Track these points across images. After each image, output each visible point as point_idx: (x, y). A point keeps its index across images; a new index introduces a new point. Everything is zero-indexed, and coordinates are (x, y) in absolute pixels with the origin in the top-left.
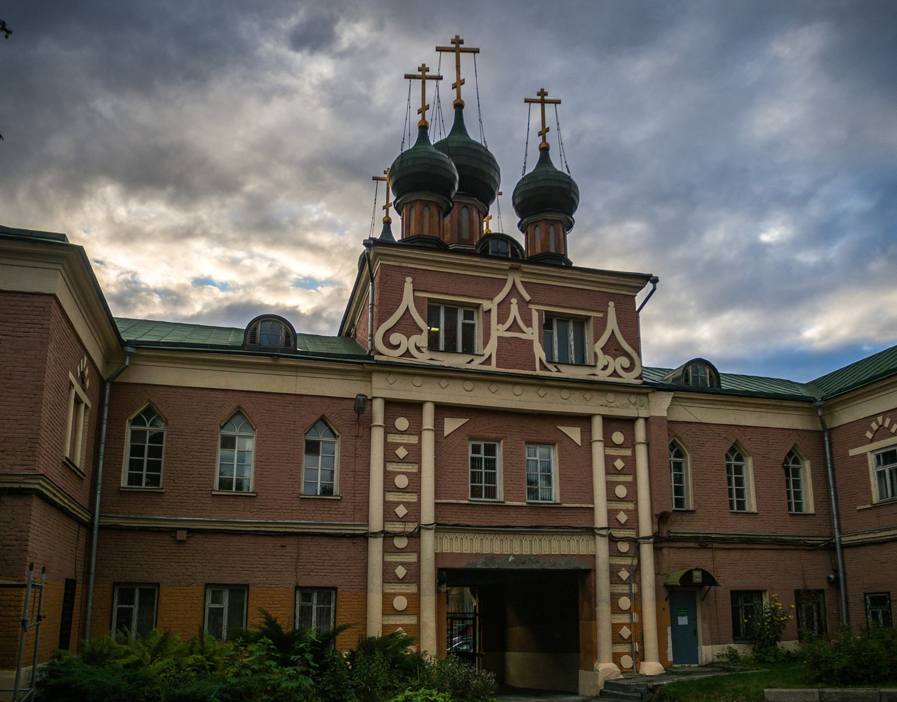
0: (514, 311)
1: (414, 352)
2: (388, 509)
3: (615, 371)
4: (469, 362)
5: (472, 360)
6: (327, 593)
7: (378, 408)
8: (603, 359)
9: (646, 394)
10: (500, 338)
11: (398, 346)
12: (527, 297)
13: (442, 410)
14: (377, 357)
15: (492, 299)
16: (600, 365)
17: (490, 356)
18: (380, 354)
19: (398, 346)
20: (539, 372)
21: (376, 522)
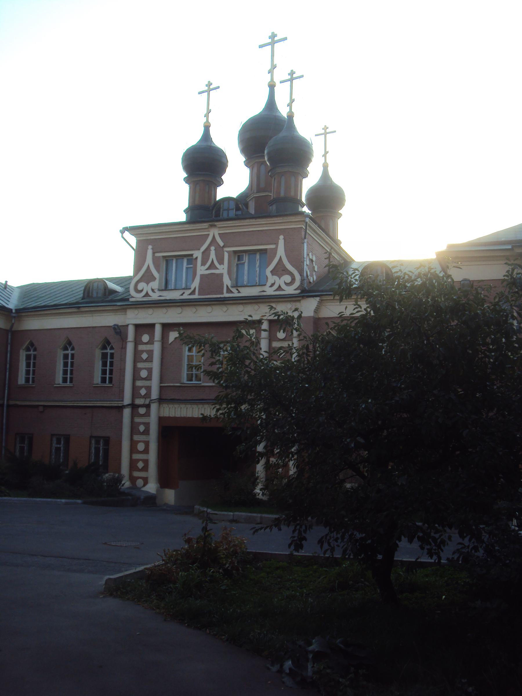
0: (213, 255)
1: (150, 293)
2: (135, 390)
3: (280, 286)
4: (182, 295)
5: (184, 293)
6: (107, 440)
7: (131, 332)
8: (272, 279)
9: (300, 300)
10: (202, 276)
11: (142, 291)
12: (222, 244)
13: (167, 327)
14: (131, 300)
15: (199, 249)
16: (269, 284)
17: (195, 289)
18: (133, 297)
19: (142, 291)
20: (226, 295)
21: (127, 399)
